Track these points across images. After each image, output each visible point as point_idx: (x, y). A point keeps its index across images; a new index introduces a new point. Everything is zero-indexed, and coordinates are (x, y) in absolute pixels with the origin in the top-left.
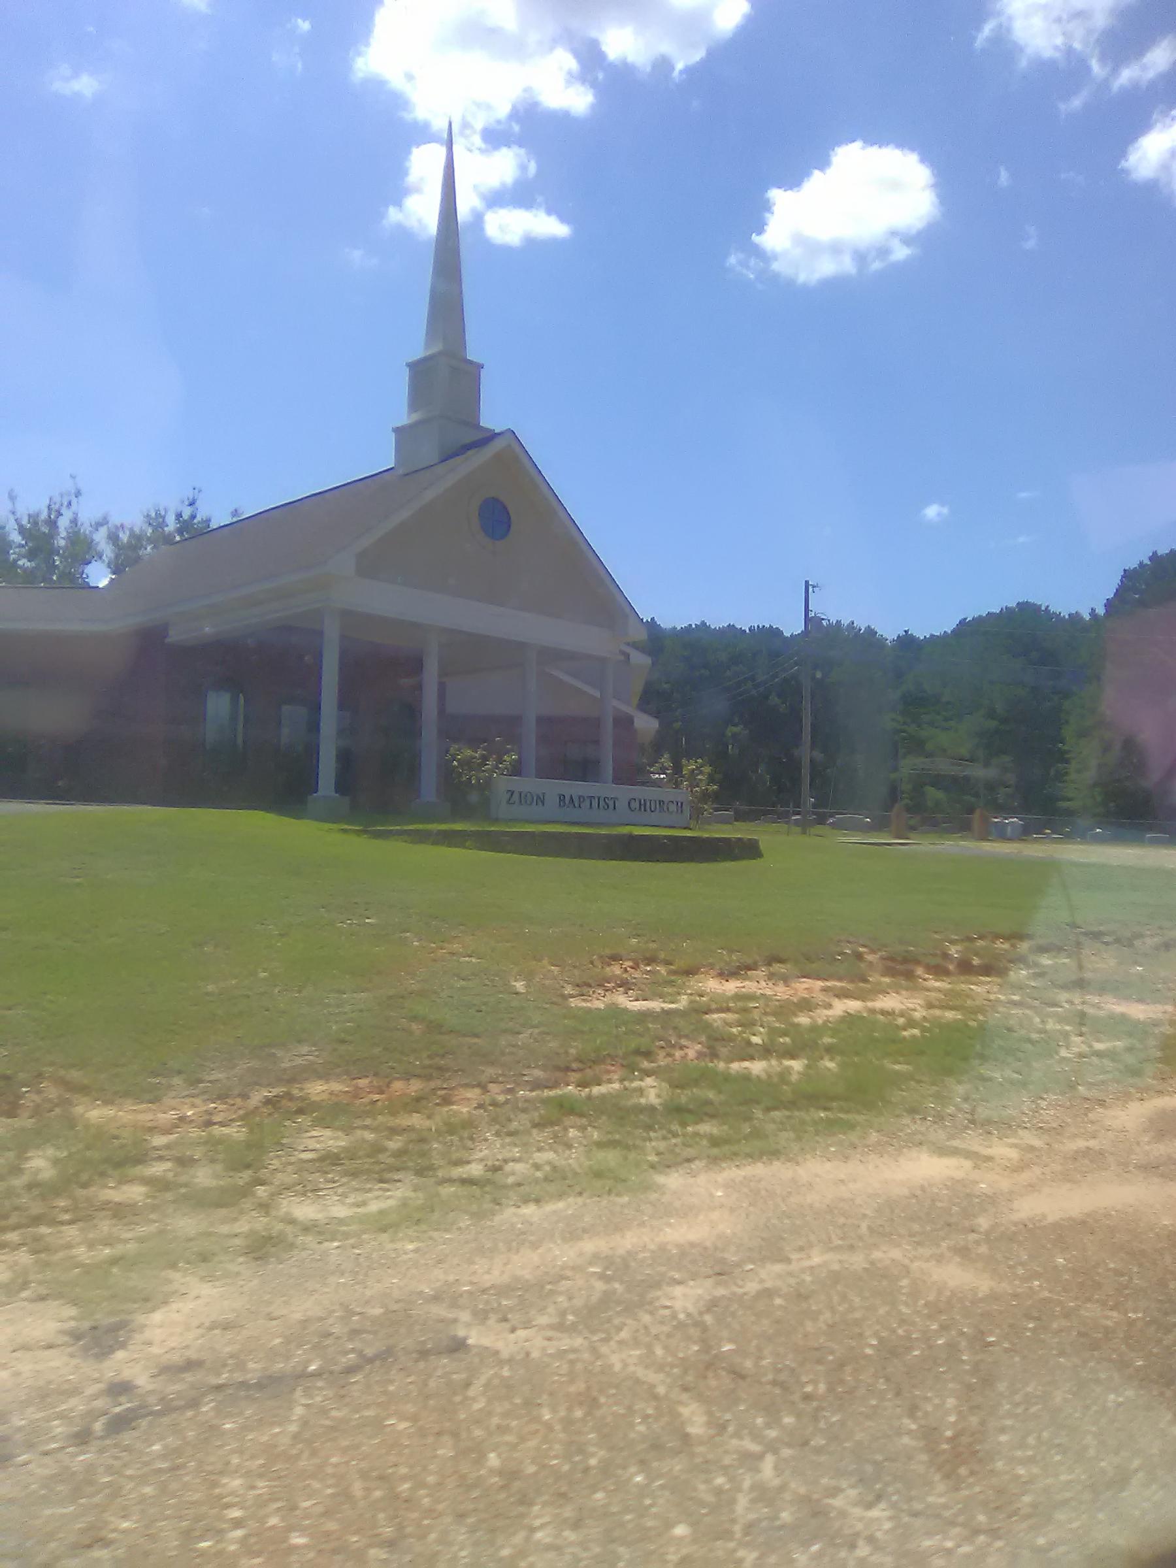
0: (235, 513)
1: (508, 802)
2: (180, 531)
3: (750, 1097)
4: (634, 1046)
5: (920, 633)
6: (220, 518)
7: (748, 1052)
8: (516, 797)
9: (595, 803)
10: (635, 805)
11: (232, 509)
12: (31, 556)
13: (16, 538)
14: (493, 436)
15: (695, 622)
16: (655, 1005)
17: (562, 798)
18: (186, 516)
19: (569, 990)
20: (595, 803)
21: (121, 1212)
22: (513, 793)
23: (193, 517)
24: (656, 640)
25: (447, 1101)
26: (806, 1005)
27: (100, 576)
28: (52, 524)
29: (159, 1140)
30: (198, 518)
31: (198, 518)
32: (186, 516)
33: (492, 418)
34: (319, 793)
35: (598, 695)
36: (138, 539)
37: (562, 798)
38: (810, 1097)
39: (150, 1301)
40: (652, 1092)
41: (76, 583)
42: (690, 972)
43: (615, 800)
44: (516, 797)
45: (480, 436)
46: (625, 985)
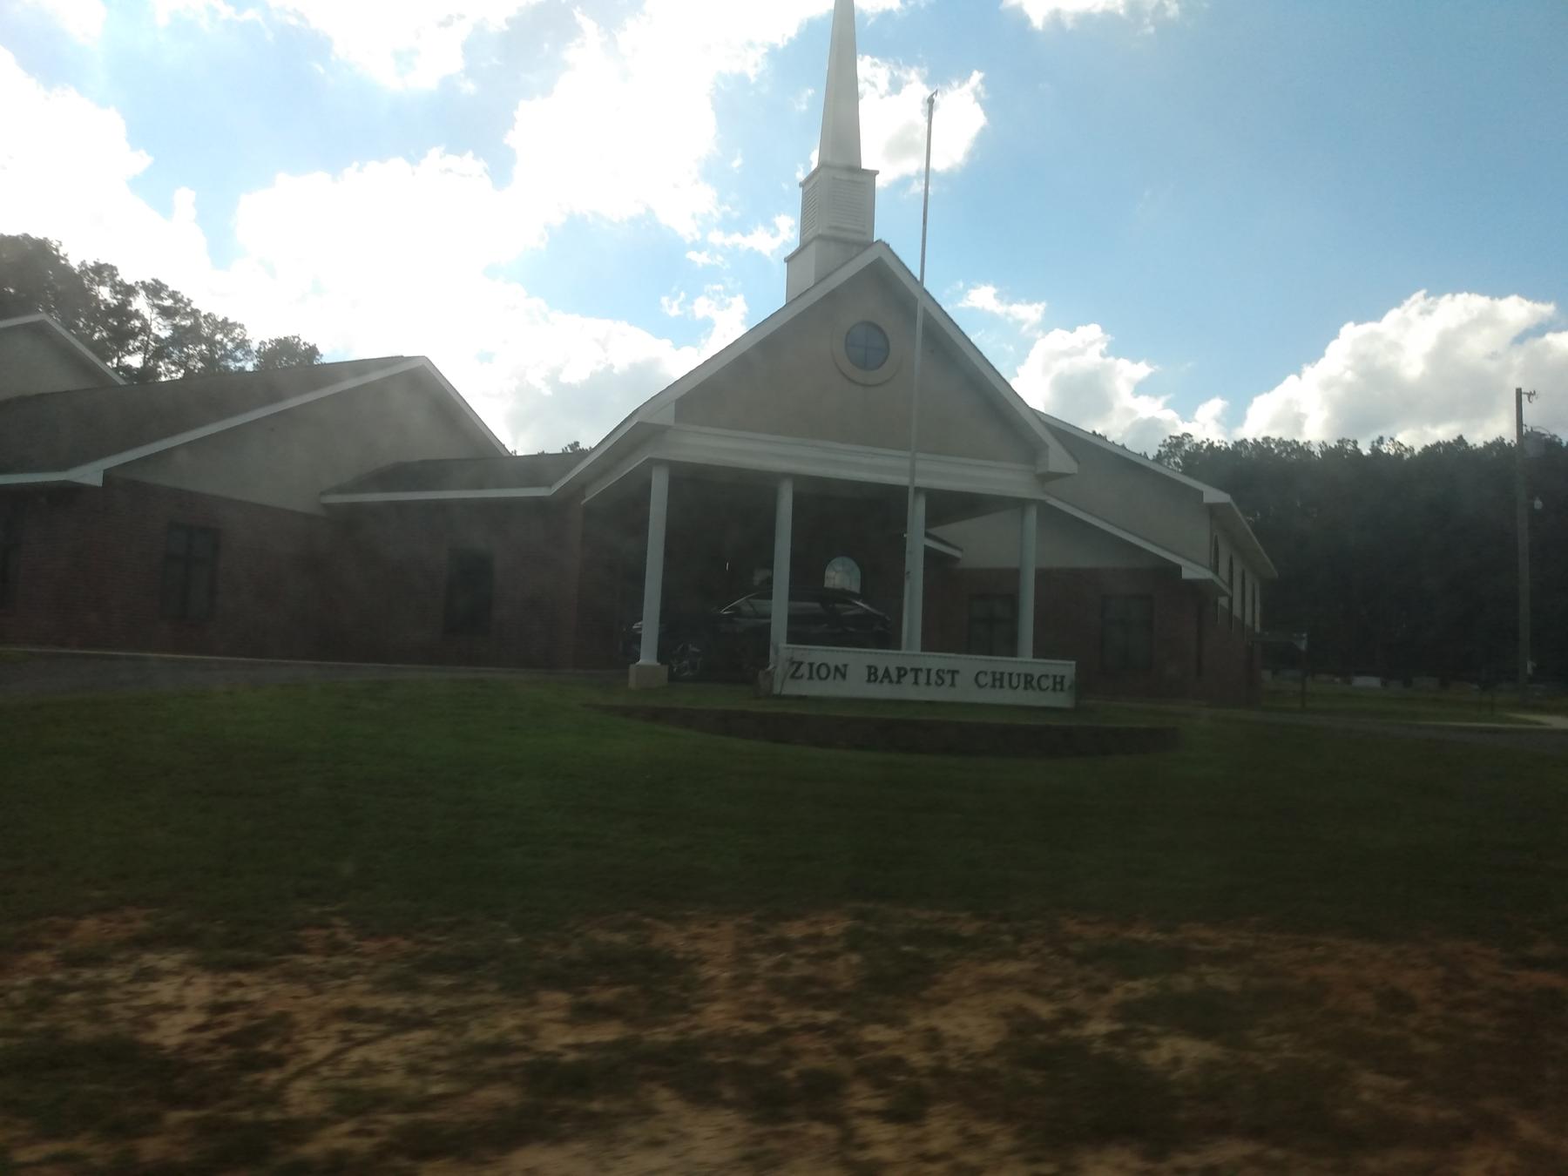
8: (804, 670)
43: (954, 673)
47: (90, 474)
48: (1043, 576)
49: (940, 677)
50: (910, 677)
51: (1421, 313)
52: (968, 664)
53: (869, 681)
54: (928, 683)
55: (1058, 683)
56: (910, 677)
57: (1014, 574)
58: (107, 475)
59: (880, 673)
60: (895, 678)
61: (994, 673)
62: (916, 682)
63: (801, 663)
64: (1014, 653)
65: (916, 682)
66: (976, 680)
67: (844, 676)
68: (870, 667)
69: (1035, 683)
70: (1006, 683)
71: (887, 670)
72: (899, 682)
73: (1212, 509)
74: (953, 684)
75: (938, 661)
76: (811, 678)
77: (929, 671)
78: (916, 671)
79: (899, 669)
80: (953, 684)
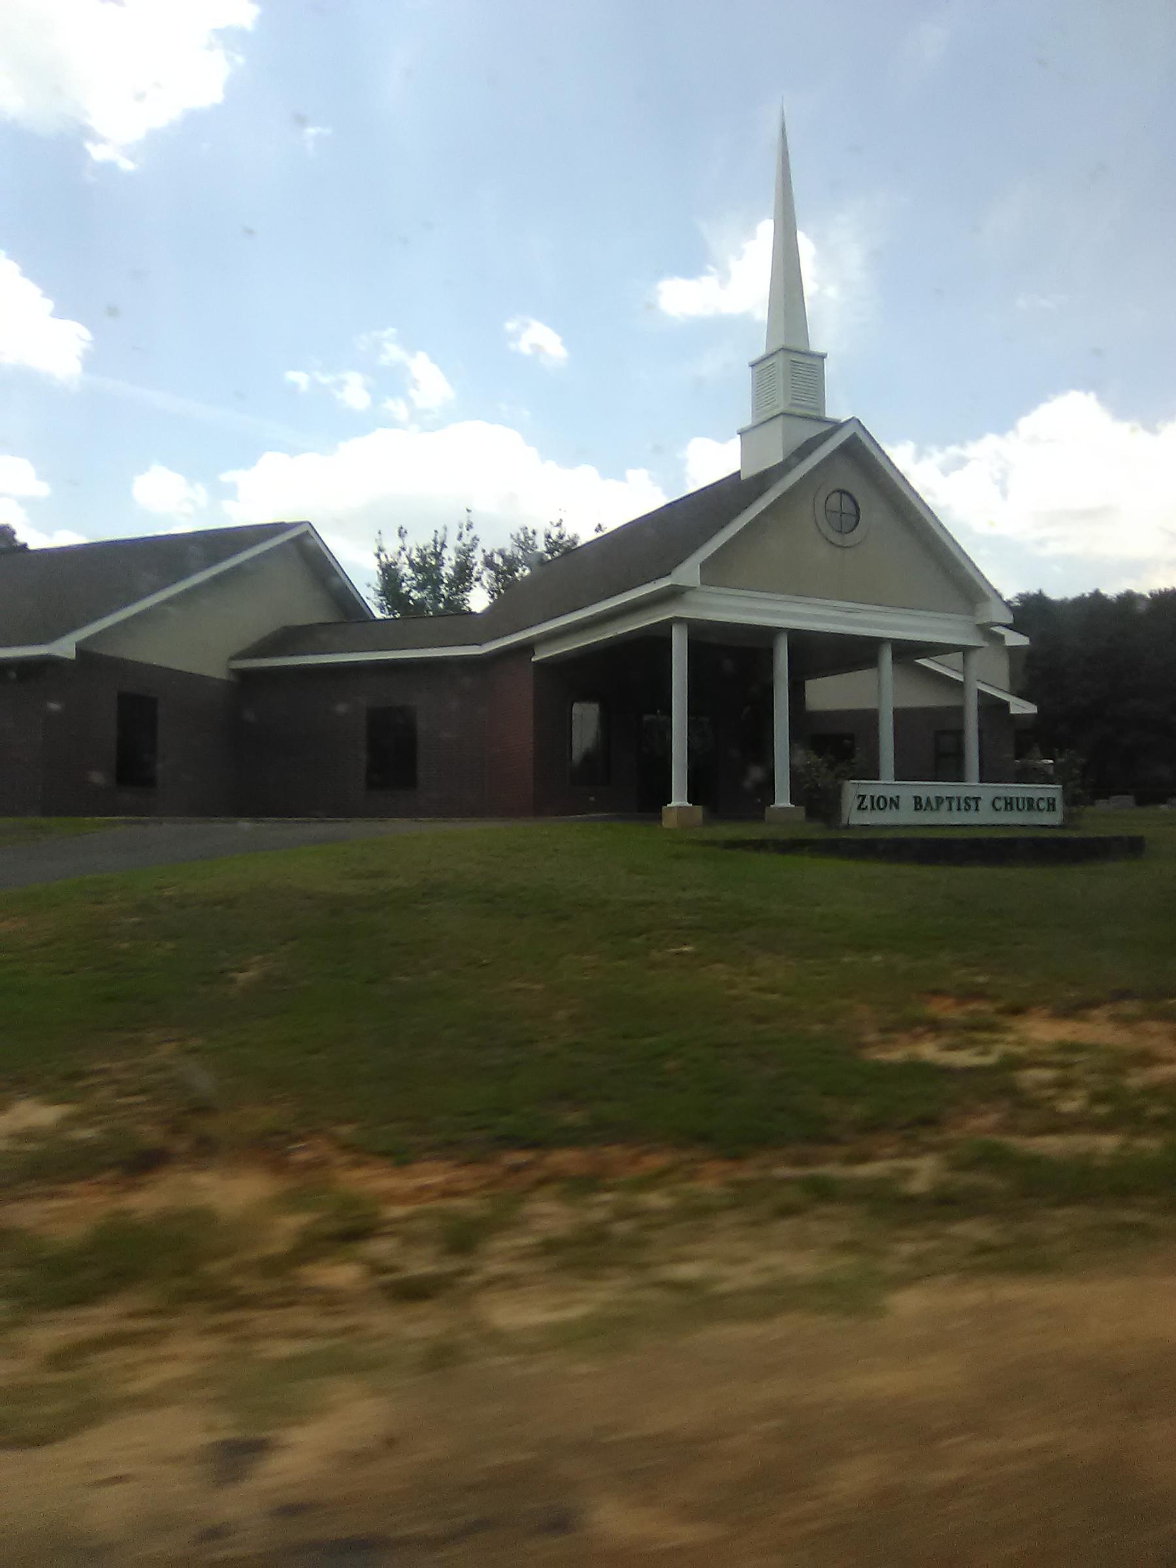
0: (599, 528)
1: (859, 808)
2: (550, 552)
3: (1045, 1185)
4: (915, 1107)
5: (1055, 593)
6: (586, 535)
7: (1060, 1125)
8: (867, 803)
9: (954, 805)
10: (1000, 804)
11: (596, 526)
12: (420, 587)
13: (407, 571)
14: (837, 426)
15: (1087, 591)
16: (964, 1058)
17: (917, 799)
18: (554, 537)
19: (872, 1037)
20: (954, 805)
21: (331, 1301)
22: (864, 797)
23: (561, 537)
24: (1033, 611)
25: (691, 1176)
26: (1146, 1059)
27: (478, 600)
28: (437, 555)
29: (397, 1211)
30: (566, 538)
31: (566, 538)
32: (554, 537)
33: (837, 408)
34: (673, 804)
35: (960, 678)
36: (511, 564)
37: (917, 799)
38: (1079, 1184)
39: (295, 1414)
40: (924, 1172)
41: (456, 611)
42: (1017, 1011)
43: (977, 799)
44: (867, 803)
45: (826, 428)
46: (935, 1027)
47: (65, 648)
48: (900, 715)
49: (966, 803)
50: (946, 804)
51: (945, 472)
52: (929, 789)
53: (916, 809)
54: (959, 809)
55: (1051, 805)
56: (946, 804)
57: (870, 718)
58: (80, 649)
59: (924, 802)
60: (934, 805)
61: (1048, 799)
62: (950, 809)
63: (864, 797)
64: (960, 779)
65: (950, 809)
66: (993, 804)
67: (897, 807)
68: (915, 798)
69: (1035, 805)
70: (1015, 807)
71: (928, 799)
72: (938, 808)
73: (1013, 651)
74: (977, 809)
75: (989, 791)
76: (873, 808)
77: (959, 799)
78: (950, 799)
79: (937, 798)
80: (977, 809)
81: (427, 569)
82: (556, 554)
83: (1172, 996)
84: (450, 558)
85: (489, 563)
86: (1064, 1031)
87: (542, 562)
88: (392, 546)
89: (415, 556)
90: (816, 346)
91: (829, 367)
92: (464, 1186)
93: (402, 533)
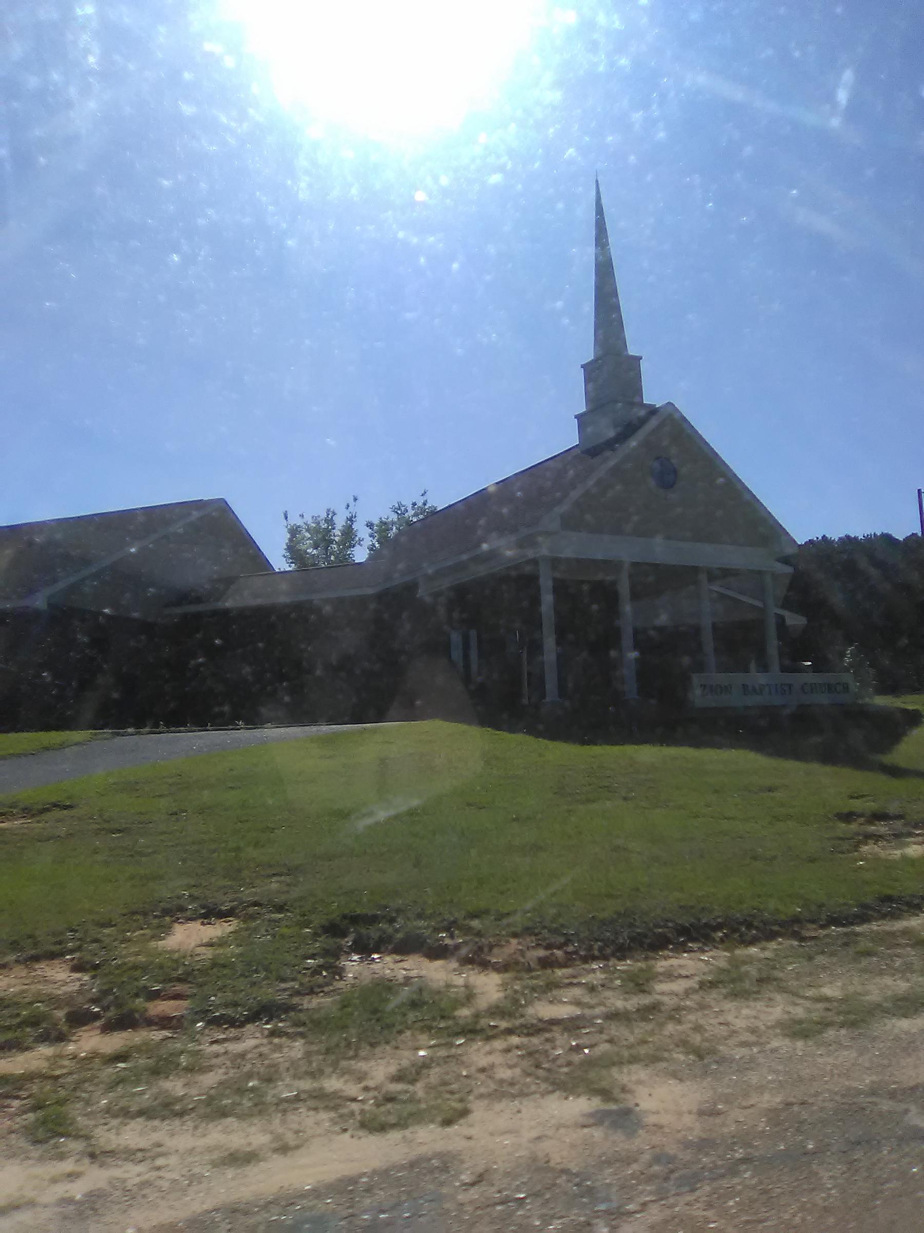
2: (416, 515)
14: (653, 411)
18: (420, 504)
33: (652, 396)
41: (344, 561)
45: (642, 413)
57: (697, 630)
81: (323, 537)
82: (421, 517)
83: (914, 906)
84: (340, 522)
85: (370, 525)
86: (525, 1040)
87: (409, 524)
88: (295, 520)
89: (310, 521)
90: (632, 351)
91: (644, 366)
92: (392, 1119)
93: (302, 516)
